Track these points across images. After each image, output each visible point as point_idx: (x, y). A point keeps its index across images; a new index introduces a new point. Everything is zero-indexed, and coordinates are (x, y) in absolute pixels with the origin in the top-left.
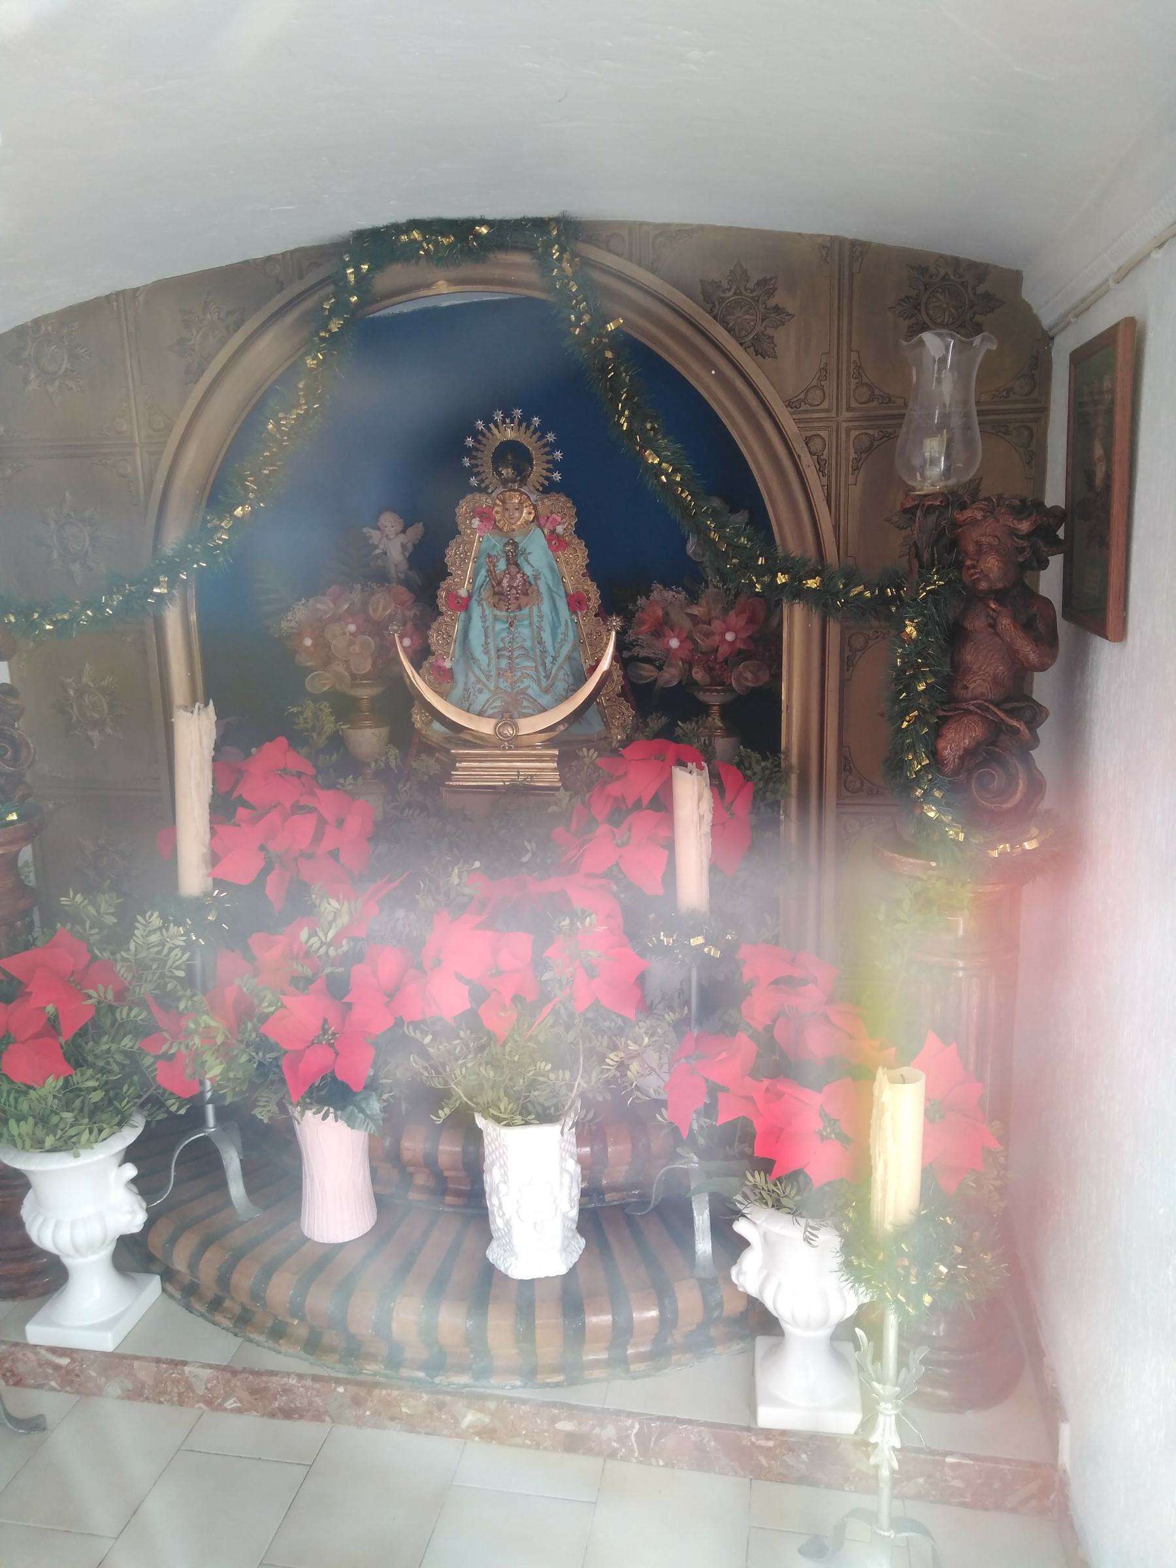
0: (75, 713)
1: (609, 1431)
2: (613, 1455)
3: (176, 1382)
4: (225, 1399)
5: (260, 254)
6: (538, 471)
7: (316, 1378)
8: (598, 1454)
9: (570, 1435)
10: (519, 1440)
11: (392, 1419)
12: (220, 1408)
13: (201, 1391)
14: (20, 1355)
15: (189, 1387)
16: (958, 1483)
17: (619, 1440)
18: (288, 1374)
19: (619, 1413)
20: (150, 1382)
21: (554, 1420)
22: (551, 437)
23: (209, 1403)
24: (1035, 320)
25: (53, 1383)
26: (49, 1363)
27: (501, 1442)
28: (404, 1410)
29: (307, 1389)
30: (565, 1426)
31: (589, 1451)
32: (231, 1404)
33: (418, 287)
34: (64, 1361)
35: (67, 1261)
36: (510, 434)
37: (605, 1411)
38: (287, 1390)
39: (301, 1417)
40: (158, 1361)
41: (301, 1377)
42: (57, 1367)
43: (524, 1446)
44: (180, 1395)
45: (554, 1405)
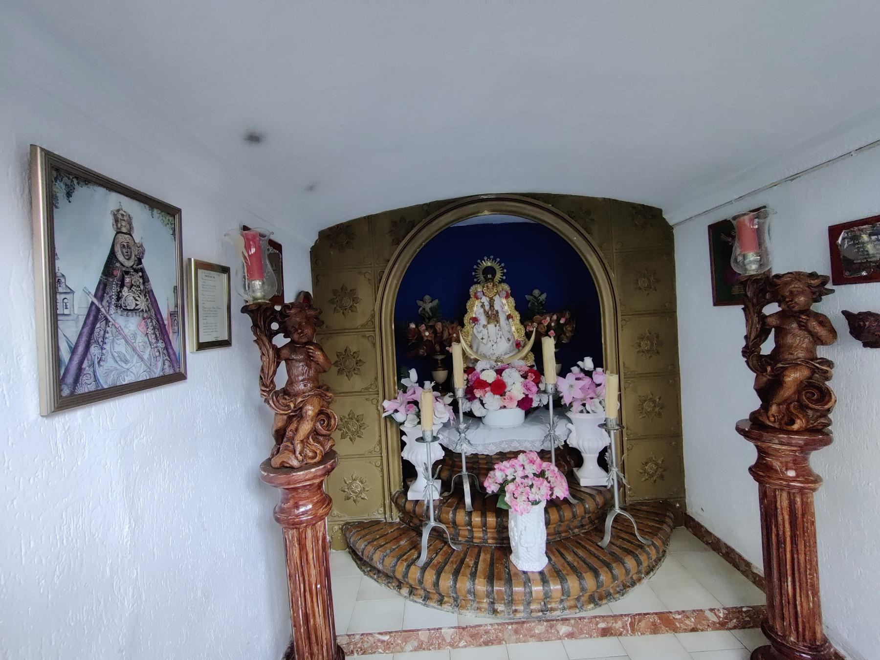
0: (652, 279)
1: (619, 625)
2: (621, 634)
3: (438, 638)
4: (460, 642)
5: (428, 202)
6: (498, 276)
7: (498, 624)
8: (615, 635)
9: (603, 629)
10: (583, 636)
11: (531, 637)
12: (458, 647)
13: (448, 640)
14: (366, 639)
15: (444, 640)
16: (747, 619)
17: (623, 627)
18: (486, 625)
19: (621, 615)
20: (426, 640)
21: (597, 624)
22: (475, 267)
23: (452, 645)
24: (667, 223)
25: (380, 650)
26: (379, 640)
27: (576, 638)
28: (537, 631)
29: (495, 629)
30: (602, 625)
31: (611, 634)
32: (462, 644)
33: (478, 212)
34: (386, 638)
35: (583, 455)
36: (489, 264)
37: (615, 616)
38: (487, 632)
39: (493, 644)
40: (429, 630)
41: (491, 625)
42: (383, 642)
43: (586, 638)
44: (439, 644)
45: (595, 617)
